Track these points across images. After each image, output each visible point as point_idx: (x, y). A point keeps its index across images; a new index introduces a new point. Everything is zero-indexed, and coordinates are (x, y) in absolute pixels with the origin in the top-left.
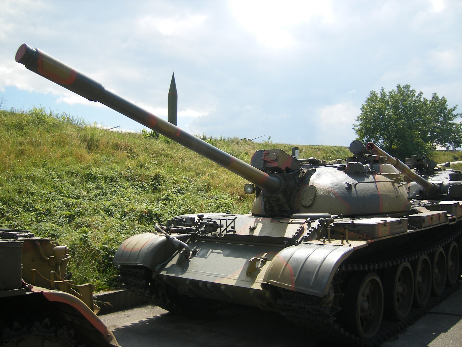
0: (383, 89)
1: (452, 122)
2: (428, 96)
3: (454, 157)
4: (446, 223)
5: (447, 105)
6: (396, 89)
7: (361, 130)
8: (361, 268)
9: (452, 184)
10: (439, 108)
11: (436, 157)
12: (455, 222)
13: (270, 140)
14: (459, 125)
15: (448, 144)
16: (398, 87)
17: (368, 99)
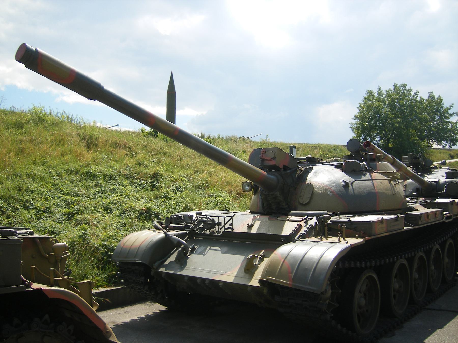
0: (379, 88)
1: (448, 120)
2: (424, 95)
3: (450, 155)
4: (442, 221)
5: (443, 104)
6: (392, 88)
7: (358, 129)
8: (358, 264)
9: (448, 182)
10: (435, 106)
11: (432, 155)
12: (451, 220)
13: (268, 139)
14: (455, 123)
15: (444, 143)
16: (395, 86)
17: (365, 98)
